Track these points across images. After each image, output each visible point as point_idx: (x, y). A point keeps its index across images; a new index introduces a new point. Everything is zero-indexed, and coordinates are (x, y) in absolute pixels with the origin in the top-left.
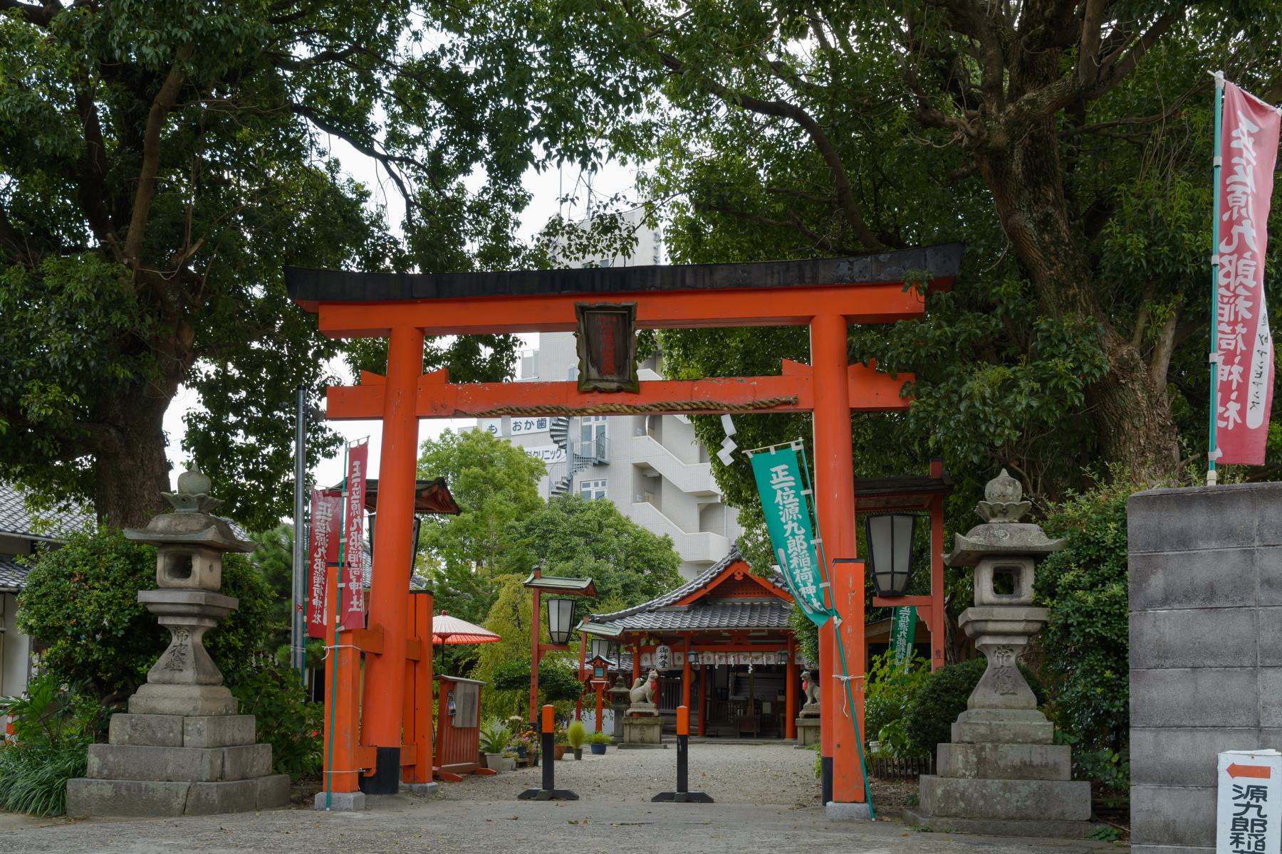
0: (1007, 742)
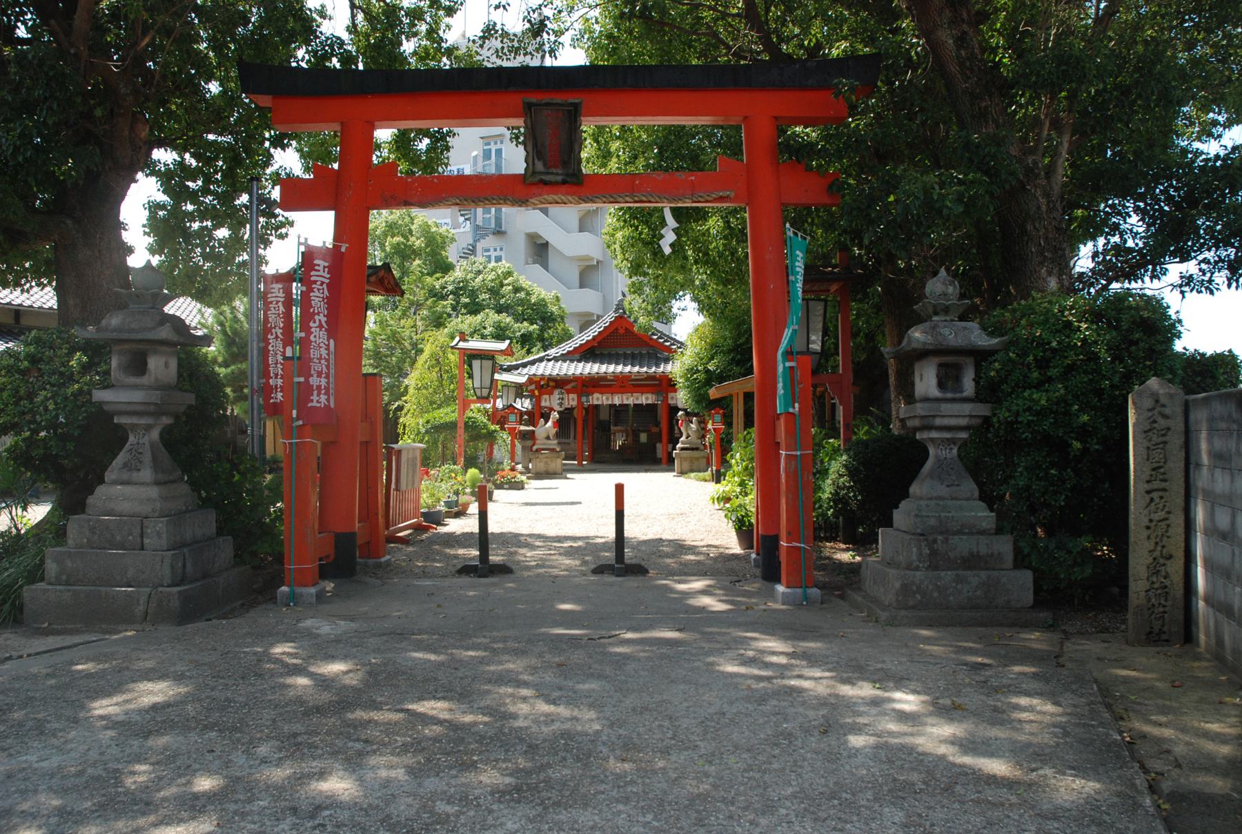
0: (955, 533)
